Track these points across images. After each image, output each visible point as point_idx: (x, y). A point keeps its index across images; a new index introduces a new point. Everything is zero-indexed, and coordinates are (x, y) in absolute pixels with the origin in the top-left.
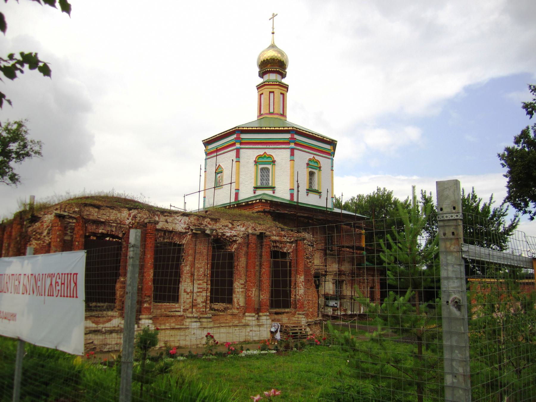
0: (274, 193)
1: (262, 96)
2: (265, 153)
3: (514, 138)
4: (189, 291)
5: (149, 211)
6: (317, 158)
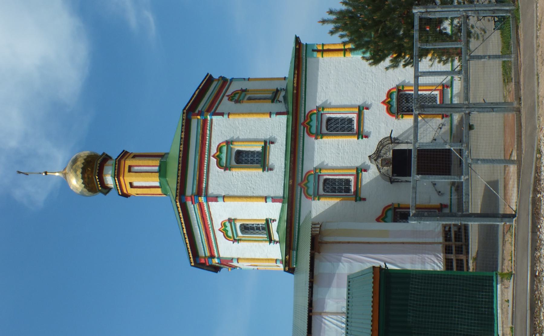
0: (274, 220)
1: (135, 184)
2: (220, 230)
3: (227, 171)
5: (238, 157)
6: (214, 151)
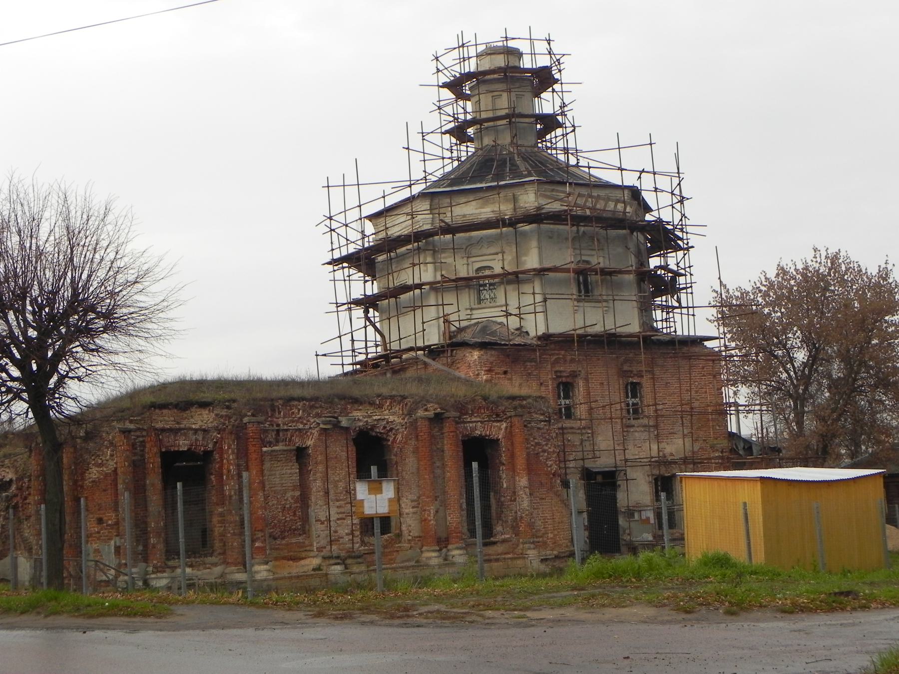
4: (323, 519)
